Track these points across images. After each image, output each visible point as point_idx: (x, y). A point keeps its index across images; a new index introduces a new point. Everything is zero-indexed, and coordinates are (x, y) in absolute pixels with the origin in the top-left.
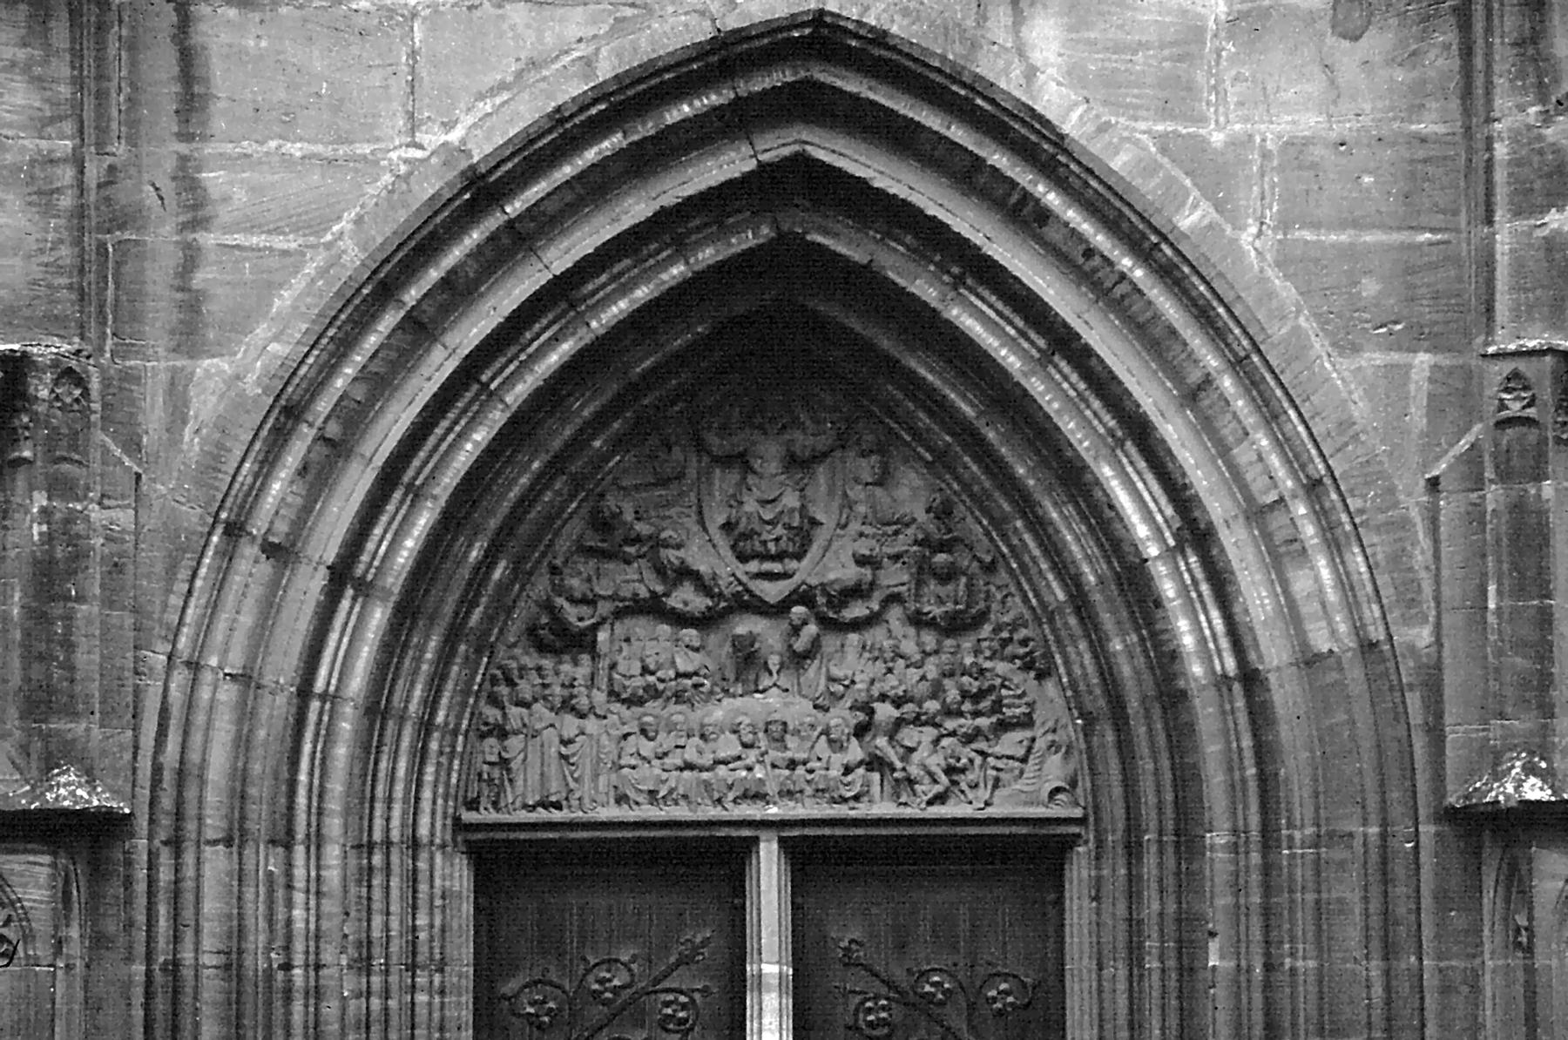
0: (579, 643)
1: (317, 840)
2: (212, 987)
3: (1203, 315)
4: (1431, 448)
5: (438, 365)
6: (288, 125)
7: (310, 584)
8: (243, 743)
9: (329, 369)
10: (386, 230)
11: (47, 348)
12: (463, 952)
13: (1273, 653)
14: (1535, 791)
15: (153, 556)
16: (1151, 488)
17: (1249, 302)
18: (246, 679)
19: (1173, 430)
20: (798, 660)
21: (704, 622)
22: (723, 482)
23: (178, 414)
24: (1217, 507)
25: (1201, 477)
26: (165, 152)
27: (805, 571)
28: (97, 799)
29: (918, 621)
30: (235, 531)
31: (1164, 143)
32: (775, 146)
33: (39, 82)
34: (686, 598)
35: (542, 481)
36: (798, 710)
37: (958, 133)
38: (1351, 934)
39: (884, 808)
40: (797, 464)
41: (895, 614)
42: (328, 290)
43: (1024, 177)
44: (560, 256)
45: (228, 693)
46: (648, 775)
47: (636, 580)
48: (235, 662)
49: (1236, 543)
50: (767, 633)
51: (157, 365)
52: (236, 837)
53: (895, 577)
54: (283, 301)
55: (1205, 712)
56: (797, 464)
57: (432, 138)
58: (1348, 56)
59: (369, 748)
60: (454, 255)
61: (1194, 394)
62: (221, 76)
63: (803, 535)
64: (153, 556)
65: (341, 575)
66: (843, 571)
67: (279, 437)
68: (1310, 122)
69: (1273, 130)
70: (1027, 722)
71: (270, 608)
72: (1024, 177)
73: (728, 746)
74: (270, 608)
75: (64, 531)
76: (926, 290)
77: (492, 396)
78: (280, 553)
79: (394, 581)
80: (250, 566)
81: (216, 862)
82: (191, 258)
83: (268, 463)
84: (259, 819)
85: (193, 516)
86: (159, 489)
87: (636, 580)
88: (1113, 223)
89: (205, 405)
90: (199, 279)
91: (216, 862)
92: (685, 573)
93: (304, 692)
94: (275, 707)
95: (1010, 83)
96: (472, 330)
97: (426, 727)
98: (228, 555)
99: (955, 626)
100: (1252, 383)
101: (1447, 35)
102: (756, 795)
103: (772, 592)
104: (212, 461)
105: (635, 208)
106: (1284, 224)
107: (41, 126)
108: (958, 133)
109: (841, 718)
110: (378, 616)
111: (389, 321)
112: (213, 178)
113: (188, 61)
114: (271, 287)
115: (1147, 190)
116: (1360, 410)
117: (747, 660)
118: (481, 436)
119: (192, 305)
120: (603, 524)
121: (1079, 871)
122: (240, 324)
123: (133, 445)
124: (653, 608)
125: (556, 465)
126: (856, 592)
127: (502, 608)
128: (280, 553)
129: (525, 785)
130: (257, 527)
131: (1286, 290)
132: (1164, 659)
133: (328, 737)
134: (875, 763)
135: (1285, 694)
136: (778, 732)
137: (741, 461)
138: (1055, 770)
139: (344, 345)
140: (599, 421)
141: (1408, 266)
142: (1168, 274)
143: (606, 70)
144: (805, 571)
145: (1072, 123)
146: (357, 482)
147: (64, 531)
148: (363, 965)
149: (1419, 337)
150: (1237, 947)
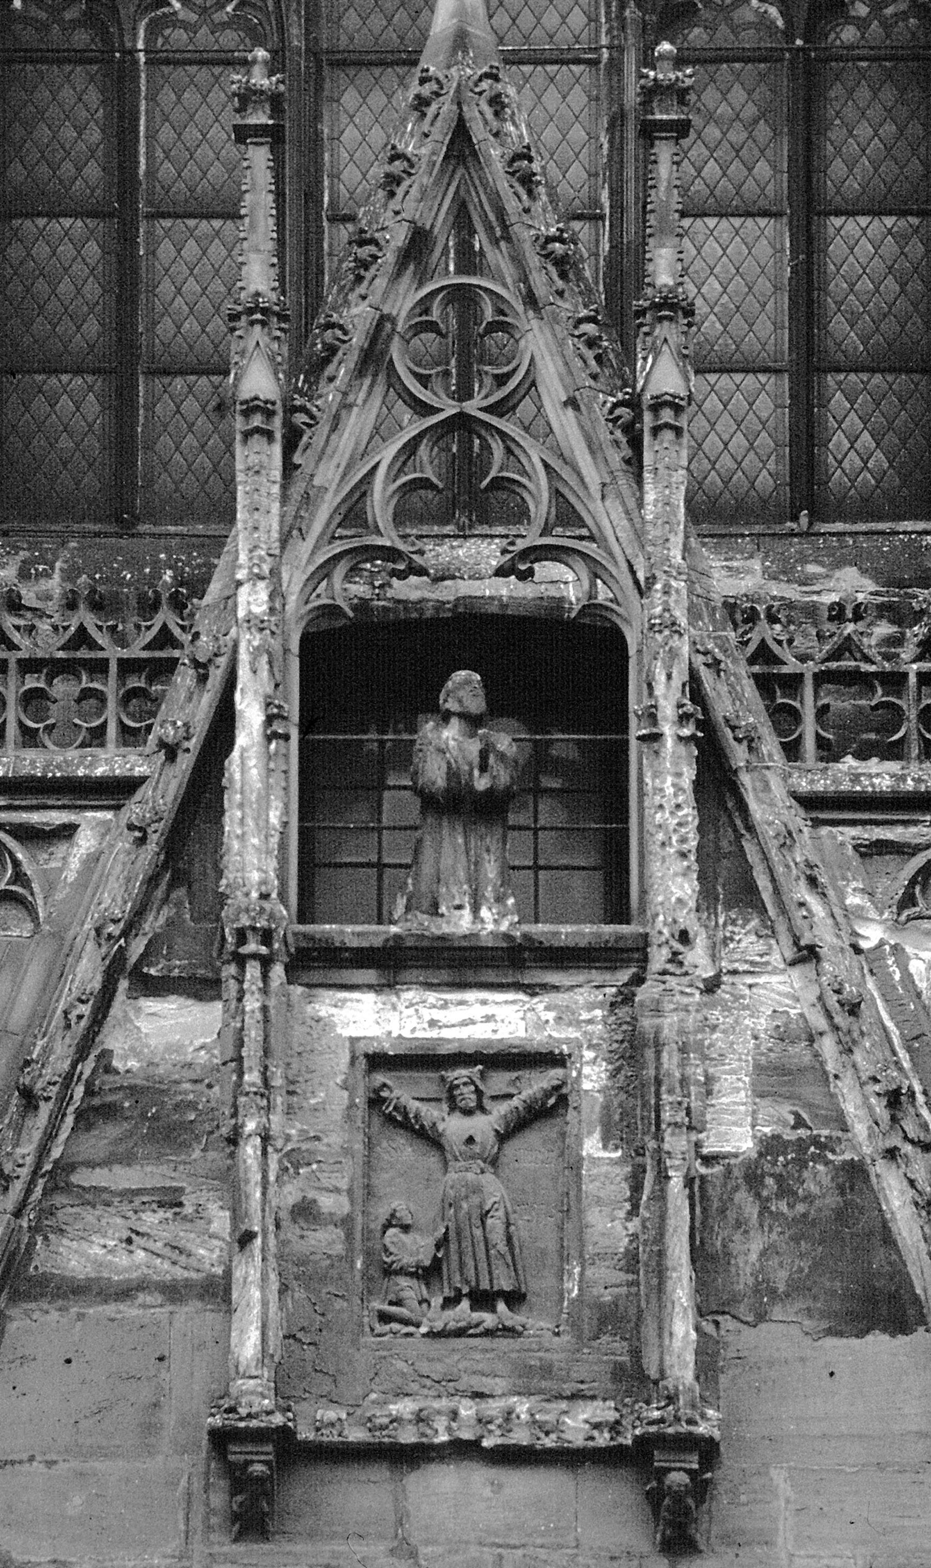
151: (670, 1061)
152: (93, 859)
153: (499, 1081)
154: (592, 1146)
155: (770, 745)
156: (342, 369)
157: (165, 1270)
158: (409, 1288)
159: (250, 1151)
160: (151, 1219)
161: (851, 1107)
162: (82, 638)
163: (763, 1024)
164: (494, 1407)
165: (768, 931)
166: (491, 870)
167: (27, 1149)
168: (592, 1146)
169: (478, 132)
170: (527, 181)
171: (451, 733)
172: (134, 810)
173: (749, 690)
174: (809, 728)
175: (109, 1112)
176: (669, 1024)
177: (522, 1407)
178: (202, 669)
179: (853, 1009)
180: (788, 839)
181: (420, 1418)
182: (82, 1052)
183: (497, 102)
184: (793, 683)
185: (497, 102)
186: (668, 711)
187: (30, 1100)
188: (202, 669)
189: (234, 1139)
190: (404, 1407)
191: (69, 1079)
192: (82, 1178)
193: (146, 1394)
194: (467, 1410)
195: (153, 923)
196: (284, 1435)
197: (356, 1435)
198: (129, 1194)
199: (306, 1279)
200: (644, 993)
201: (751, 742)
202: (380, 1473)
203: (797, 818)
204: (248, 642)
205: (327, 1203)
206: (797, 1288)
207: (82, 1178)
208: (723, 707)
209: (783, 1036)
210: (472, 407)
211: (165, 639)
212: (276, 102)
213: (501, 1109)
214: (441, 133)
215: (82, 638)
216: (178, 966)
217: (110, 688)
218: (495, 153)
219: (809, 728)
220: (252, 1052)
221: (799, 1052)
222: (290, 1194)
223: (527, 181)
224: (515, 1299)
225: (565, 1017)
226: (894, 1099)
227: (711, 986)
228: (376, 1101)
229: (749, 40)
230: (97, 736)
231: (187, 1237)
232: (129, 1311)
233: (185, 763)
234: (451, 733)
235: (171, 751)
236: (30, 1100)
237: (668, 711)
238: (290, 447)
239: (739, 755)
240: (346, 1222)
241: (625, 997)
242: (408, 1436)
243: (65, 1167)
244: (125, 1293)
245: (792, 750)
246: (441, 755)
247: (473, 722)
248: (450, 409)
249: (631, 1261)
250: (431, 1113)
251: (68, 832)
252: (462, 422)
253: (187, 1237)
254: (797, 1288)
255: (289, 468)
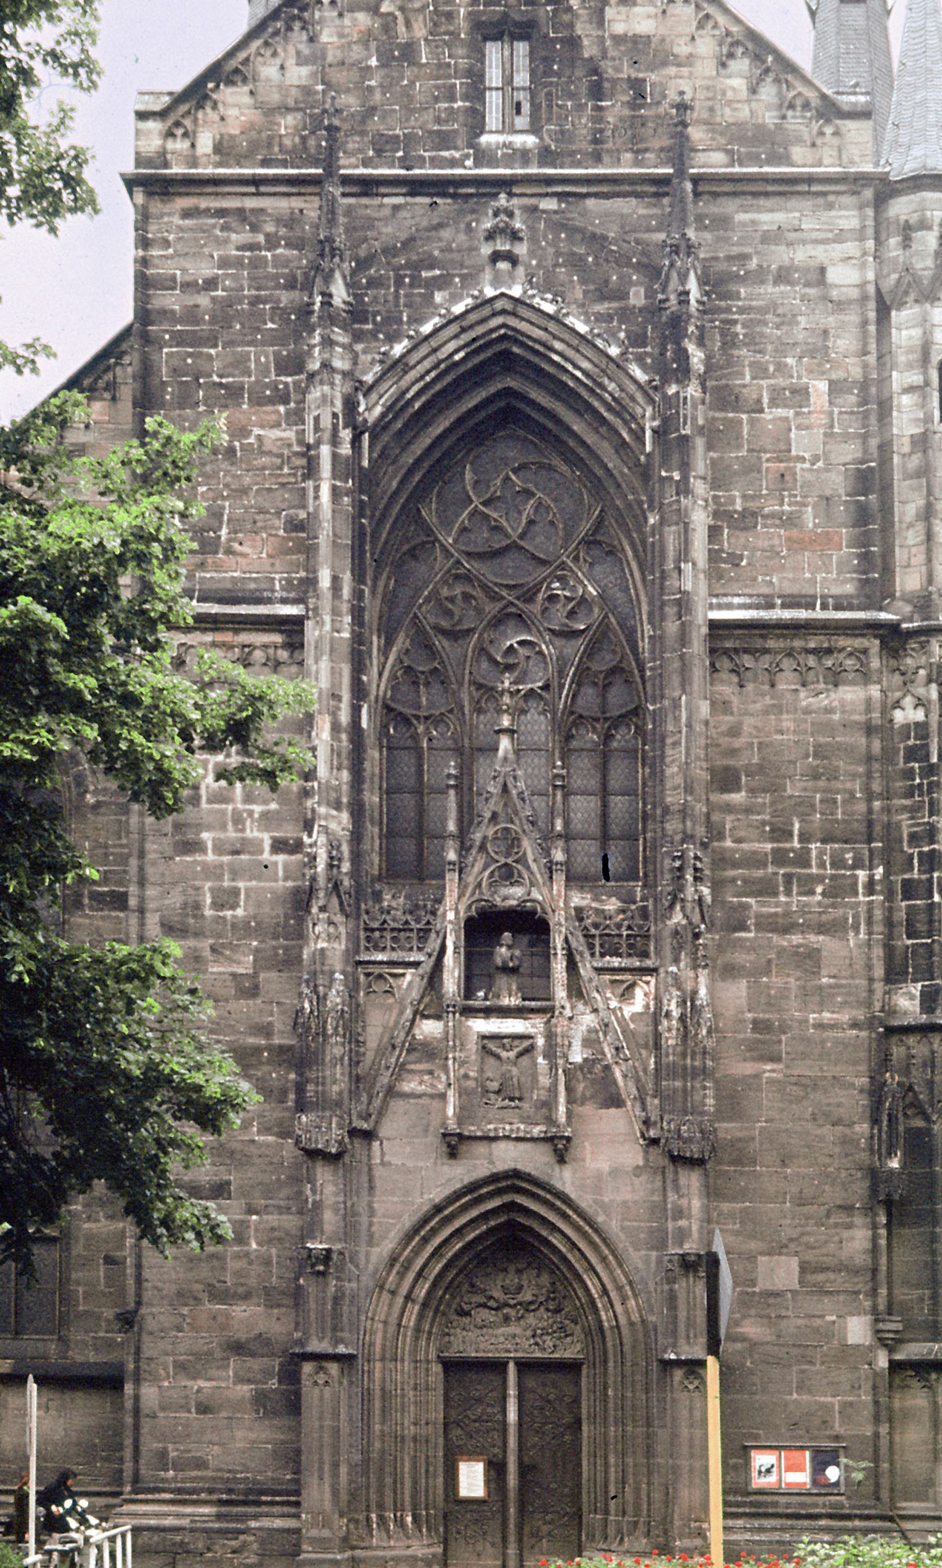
0: (467, 1314)
1: (403, 1360)
2: (378, 1393)
3: (604, 1240)
4: (655, 1276)
5: (429, 1249)
6: (393, 1193)
7: (400, 1300)
8: (384, 1338)
9: (404, 1250)
10: (415, 1219)
11: (337, 1247)
12: (441, 1387)
13: (623, 1320)
14: (673, 1357)
15: (362, 1294)
16: (596, 1281)
17: (614, 1239)
18: (385, 1323)
19: (599, 1268)
20: (519, 1319)
21: (496, 1309)
22: (501, 1276)
23: (367, 1261)
24: (609, 1286)
25: (606, 1279)
26: (365, 1199)
27: (520, 1297)
28: (350, 1351)
29: (548, 1310)
30: (382, 1288)
31: (595, 1201)
32: (507, 1198)
33: (336, 1185)
34: (492, 1303)
35: (457, 1275)
36: (518, 1331)
37: (548, 1196)
38: (638, 1387)
39: (538, 1355)
40: (519, 1271)
41: (542, 1309)
42: (401, 1235)
43: (564, 1207)
44: (458, 1223)
45: (380, 1326)
46: (482, 1346)
47: (480, 1299)
48: (383, 1318)
49: (613, 1294)
50: (512, 1313)
51: (363, 1249)
52: (383, 1359)
53: (542, 1299)
54: (392, 1234)
55: (608, 1333)
56: (519, 1271)
57: (426, 1196)
58: (637, 1181)
59: (417, 1339)
60: (433, 1223)
61: (604, 1259)
62: (378, 1183)
63: (520, 1288)
64: (362, 1294)
65: (408, 1298)
66: (529, 1298)
67: (392, 1266)
68: (628, 1197)
69: (619, 1199)
70: (572, 1335)
71: (390, 1306)
72: (564, 1207)
73: (502, 1339)
74: (390, 1306)
75: (339, 1289)
76: (544, 1233)
77: (442, 1256)
78: (393, 1293)
79: (420, 1300)
80: (386, 1296)
81: (378, 1365)
82: (371, 1224)
83: (388, 1274)
84: (388, 1356)
85: (371, 1284)
86: (363, 1278)
87: (480, 1299)
88: (585, 1219)
89: (374, 1259)
90: (374, 1229)
91: (378, 1365)
92: (491, 1297)
93: (399, 1325)
94: (392, 1329)
95: (559, 1185)
96: (437, 1241)
97: (430, 1333)
98: (380, 1293)
99: (557, 1311)
100: (616, 1257)
101: (659, 1177)
102: (509, 1351)
103: (512, 1302)
104: (376, 1271)
105: (474, 1213)
106: (623, 1220)
107: (337, 1195)
108: (548, 1196)
109: (529, 1333)
110: (417, 1308)
111: (417, 1238)
112: (375, 1205)
113: (371, 1180)
114: (389, 1231)
115: (590, 1212)
116: (640, 1265)
117: (507, 1319)
118: (440, 1265)
119: (371, 1236)
120: (472, 1285)
121: (584, 1371)
122: (384, 1238)
123: (357, 1266)
124: (485, 1306)
125: (461, 1271)
126: (532, 1303)
127: (449, 1305)
128: (393, 1293)
129: (455, 1348)
130: (387, 1286)
131: (623, 1237)
132: (600, 1322)
133: (405, 1336)
134: (537, 1344)
135: (625, 1332)
136: (514, 1336)
137: (505, 1270)
138: (579, 1346)
139: (407, 1244)
140: (470, 1261)
141: (651, 1231)
142: (596, 1230)
143: (466, 1181)
144: (520, 1297)
145: (573, 1196)
146: (411, 1276)
147: (339, 1289)
148: (415, 1389)
149: (653, 1248)
150: (616, 1389)
151: (559, 1040)
152: (410, 983)
153: (516, 1043)
154: (540, 1060)
155: (587, 954)
156: (474, 851)
157: (429, 1090)
158: (492, 1096)
159: (450, 1062)
160: (426, 1077)
161: (606, 1050)
162: (407, 922)
163: (584, 1028)
164: (515, 1127)
165: (586, 1004)
166: (514, 987)
167: (393, 1060)
168: (540, 1060)
169: (510, 786)
170: (523, 800)
171: (504, 950)
172: (421, 971)
173: (581, 939)
174: (597, 949)
175: (414, 1049)
176: (559, 1030)
177: (522, 1127)
178: (438, 933)
179: (606, 1025)
180: (590, 980)
181: (496, 1130)
182: (408, 1034)
183: (515, 778)
184: (593, 936)
185: (515, 778)
186: (559, 946)
187: (394, 1047)
188: (438, 933)
189: (447, 1059)
190: (491, 1127)
191: (404, 1042)
192: (409, 1067)
193: (424, 1122)
194: (508, 1127)
195: (426, 1000)
196: (460, 1135)
197: (479, 1134)
198: (420, 1071)
199: (468, 1094)
200: (554, 1021)
201: (581, 954)
202: (485, 1143)
203: (593, 975)
204: (450, 927)
205: (472, 1074)
206: (592, 1097)
207: (409, 1067)
208: (574, 944)
209: (589, 1031)
210: (509, 861)
211: (428, 923)
212: (456, 777)
213: (516, 1050)
214: (500, 787)
215: (407, 922)
216: (432, 1011)
217: (414, 935)
218: (514, 792)
219: (597, 949)
220: (451, 1037)
221: (593, 1036)
222: (462, 1071)
223: (523, 800)
224: (520, 1099)
225: (533, 1026)
226: (617, 1049)
227: (571, 1018)
228: (484, 1047)
229: (589, 746)
230: (411, 949)
231: (436, 1083)
232: (421, 1101)
233: (433, 958)
234: (504, 950)
235: (430, 955)
236: (394, 1047)
237: (559, 946)
238: (460, 872)
239: (578, 958)
240: (476, 1079)
241: (549, 1021)
242: (492, 1134)
243: (403, 1064)
244: (420, 1096)
245: (593, 955)
246: (292, 1325)
247: (509, 947)
248: (503, 860)
249: (549, 1090)
250: (499, 1051)
251: (403, 975)
252: (506, 864)
253: (436, 1083)
254: (592, 1097)
255: (460, 879)
